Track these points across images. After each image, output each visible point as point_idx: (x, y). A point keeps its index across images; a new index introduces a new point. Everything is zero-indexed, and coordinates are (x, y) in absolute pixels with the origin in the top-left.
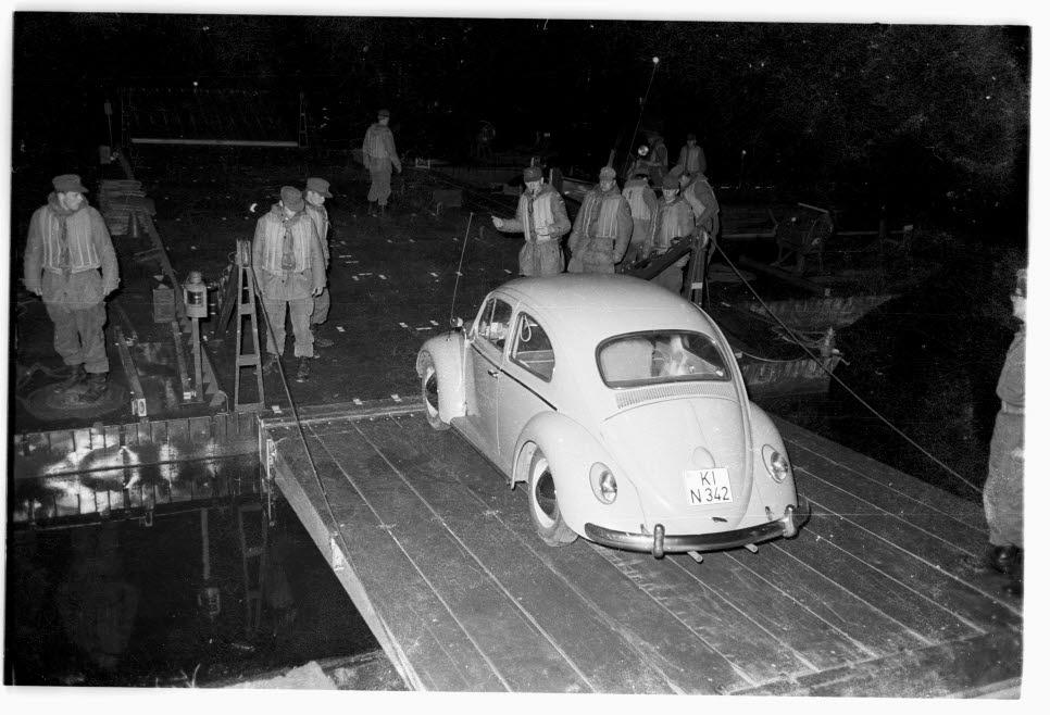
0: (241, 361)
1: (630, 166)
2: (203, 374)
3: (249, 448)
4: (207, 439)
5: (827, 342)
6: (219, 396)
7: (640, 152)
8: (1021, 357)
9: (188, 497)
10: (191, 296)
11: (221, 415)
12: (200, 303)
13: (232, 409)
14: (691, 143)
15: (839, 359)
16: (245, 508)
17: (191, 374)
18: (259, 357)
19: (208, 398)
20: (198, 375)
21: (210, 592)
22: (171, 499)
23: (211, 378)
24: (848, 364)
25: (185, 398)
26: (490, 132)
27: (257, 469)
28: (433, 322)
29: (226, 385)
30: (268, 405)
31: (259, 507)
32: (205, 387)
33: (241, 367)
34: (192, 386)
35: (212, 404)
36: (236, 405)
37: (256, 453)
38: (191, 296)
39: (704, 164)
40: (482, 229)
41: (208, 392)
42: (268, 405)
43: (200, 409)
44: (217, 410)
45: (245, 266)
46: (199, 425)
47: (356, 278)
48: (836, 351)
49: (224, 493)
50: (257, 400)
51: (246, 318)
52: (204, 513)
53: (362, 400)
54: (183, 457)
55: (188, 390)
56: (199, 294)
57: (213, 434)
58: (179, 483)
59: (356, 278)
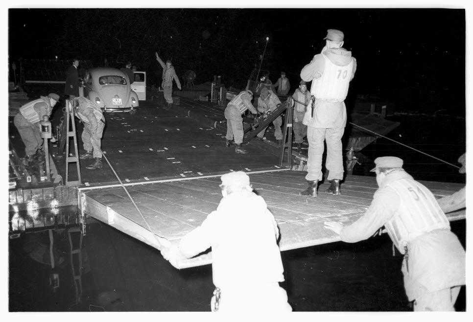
0: (68, 160)
1: (257, 86)
2: (50, 170)
3: (73, 203)
4: (52, 199)
5: (350, 153)
6: (58, 178)
7: (261, 79)
8: (353, 70)
9: (43, 225)
10: (43, 127)
11: (60, 187)
12: (48, 131)
13: (64, 184)
14: (283, 76)
15: (356, 161)
16: (70, 231)
17: (45, 169)
18: (78, 158)
19: (53, 180)
20: (48, 169)
21: (56, 276)
22: (33, 226)
23: (55, 171)
24: (360, 164)
25: (42, 180)
26: (193, 75)
27: (78, 212)
28: (165, 148)
29: (61, 173)
30: (83, 182)
31: (78, 230)
32: (51, 175)
33: (69, 163)
34: (45, 175)
35: (55, 182)
36: (67, 182)
37: (78, 205)
38: (43, 127)
39: (289, 87)
40: (189, 112)
41: (53, 177)
42: (83, 182)
43: (50, 184)
44: (57, 184)
45: (70, 112)
46: (48, 192)
47: (129, 132)
48: (355, 158)
49: (60, 223)
50: (77, 179)
51: (71, 138)
52: (50, 230)
53: (129, 179)
54: (41, 208)
55: (43, 176)
56: (48, 127)
57: (55, 197)
58: (38, 219)
59: (129, 132)
